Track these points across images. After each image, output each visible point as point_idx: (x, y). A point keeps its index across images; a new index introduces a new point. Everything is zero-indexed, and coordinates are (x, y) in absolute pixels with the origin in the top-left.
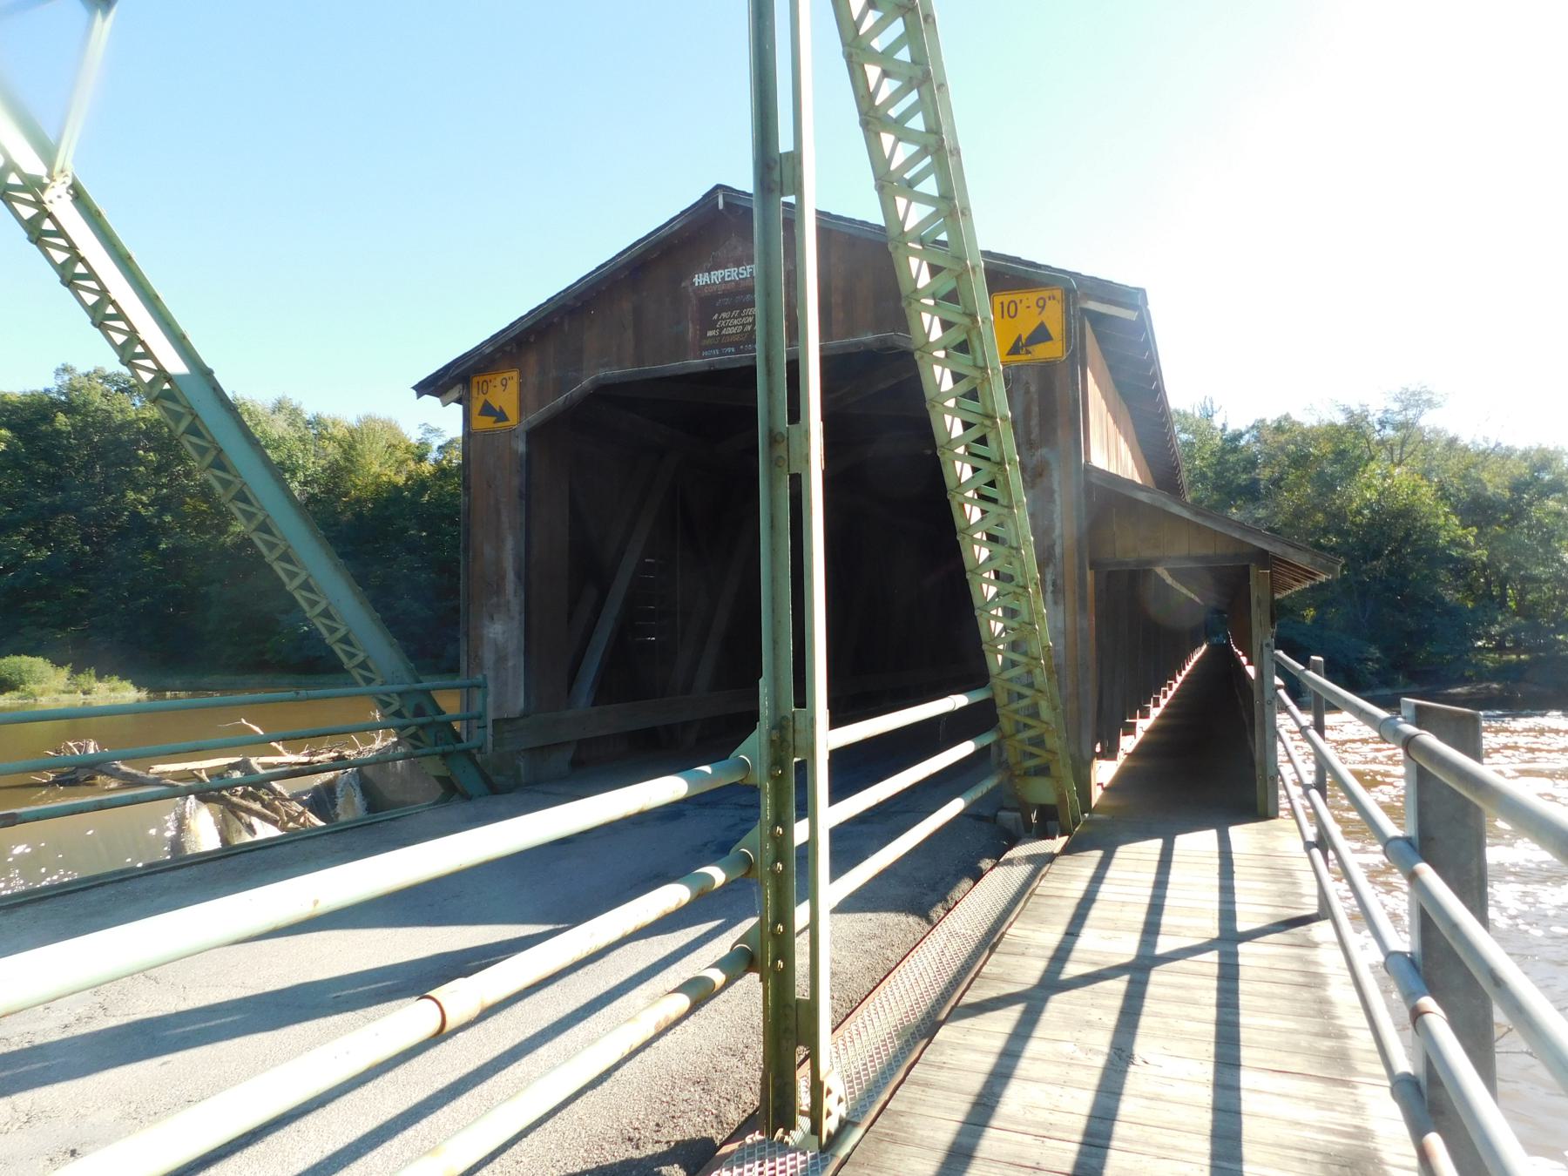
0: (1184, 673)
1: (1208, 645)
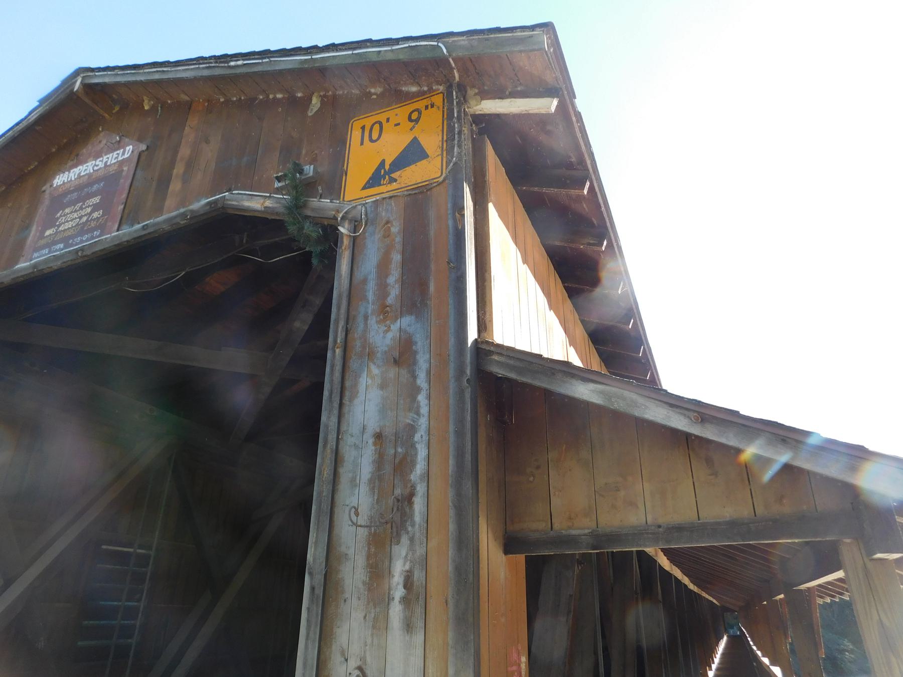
0: (714, 666)
1: (728, 636)
